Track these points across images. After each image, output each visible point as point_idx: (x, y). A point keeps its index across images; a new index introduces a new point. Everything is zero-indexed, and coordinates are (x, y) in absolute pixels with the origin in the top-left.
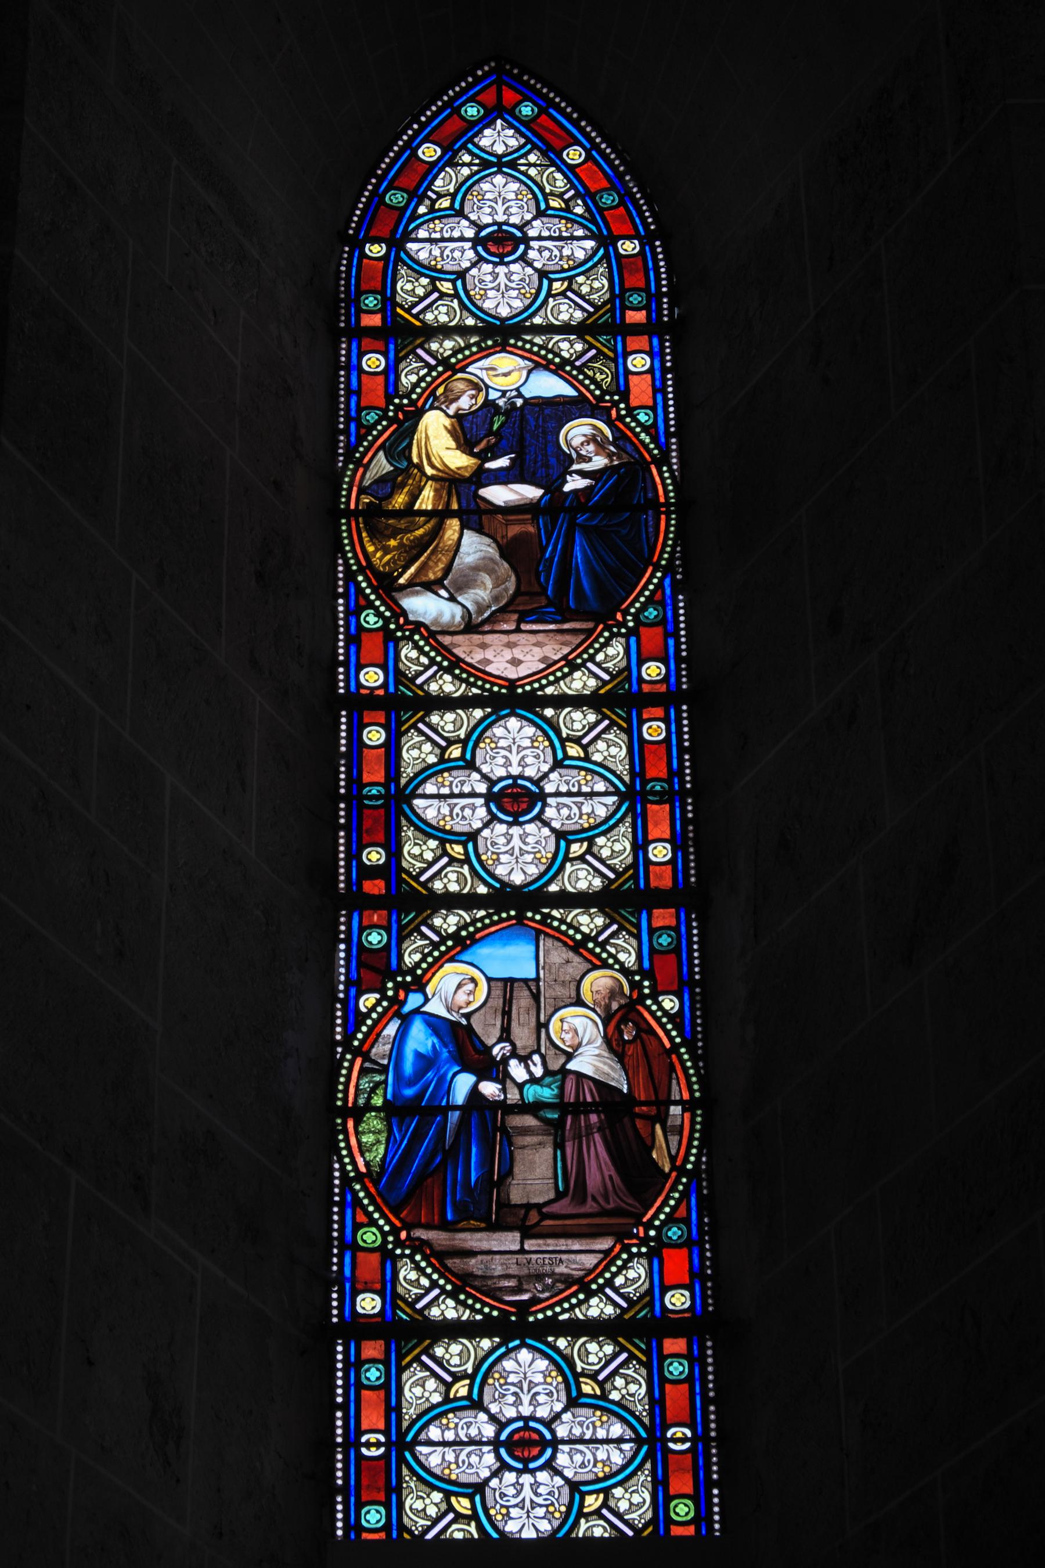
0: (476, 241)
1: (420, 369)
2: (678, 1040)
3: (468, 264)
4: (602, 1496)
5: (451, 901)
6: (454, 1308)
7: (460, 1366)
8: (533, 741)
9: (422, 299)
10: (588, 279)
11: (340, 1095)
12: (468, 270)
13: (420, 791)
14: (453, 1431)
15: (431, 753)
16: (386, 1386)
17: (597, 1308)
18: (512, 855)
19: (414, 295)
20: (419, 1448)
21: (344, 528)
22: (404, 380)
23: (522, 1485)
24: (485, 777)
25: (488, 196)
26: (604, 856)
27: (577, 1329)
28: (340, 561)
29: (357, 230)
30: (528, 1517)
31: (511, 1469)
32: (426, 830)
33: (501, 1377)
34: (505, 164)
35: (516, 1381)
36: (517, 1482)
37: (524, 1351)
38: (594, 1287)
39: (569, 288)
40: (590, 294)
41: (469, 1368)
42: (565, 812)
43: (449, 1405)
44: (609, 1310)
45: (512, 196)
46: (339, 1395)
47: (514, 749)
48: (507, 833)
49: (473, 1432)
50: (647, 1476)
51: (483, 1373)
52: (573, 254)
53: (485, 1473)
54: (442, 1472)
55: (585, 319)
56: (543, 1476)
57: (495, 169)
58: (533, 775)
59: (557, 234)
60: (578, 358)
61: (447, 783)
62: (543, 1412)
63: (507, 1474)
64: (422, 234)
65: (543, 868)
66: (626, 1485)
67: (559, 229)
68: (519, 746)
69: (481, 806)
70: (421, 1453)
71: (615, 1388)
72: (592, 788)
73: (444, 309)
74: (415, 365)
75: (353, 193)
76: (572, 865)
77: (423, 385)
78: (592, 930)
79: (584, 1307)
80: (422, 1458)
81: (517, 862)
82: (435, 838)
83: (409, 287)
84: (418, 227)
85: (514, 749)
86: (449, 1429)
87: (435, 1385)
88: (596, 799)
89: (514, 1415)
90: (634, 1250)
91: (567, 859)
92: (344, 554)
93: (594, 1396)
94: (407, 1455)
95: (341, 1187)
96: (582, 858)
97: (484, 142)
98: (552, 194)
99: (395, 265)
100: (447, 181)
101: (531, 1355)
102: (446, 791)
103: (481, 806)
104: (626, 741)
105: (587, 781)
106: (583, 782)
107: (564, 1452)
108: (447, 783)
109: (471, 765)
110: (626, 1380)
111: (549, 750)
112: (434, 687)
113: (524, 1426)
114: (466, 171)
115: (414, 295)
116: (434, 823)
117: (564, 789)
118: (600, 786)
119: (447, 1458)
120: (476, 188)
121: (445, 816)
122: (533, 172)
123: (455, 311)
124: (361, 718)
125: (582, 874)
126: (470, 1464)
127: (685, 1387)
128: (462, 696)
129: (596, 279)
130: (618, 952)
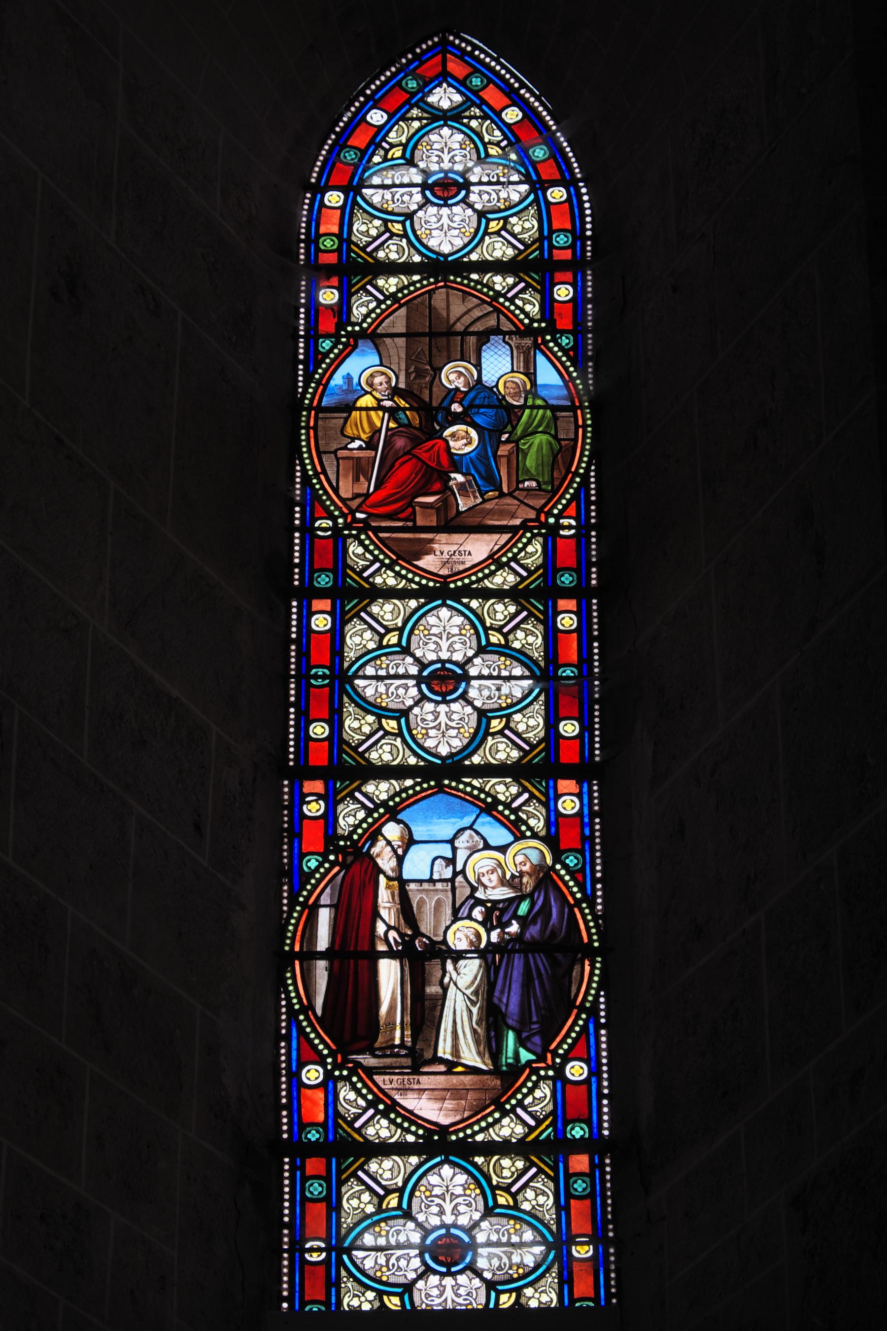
0: (424, 186)
1: (532, 1104)
2: (315, 481)
3: (415, 207)
4: (514, 1295)
5: (386, 772)
6: (387, 1128)
7: (391, 1179)
8: (427, 734)
9: (375, 239)
10: (520, 219)
11: (288, 941)
12: (415, 212)
13: (361, 673)
14: (384, 1238)
15: (518, 722)
16: (327, 1199)
17: (391, 284)
18: (449, 633)
19: (369, 236)
20: (354, 1253)
21: (304, 443)
22: (355, 311)
23: (445, 1287)
24: (417, 660)
25: (436, 146)
26: (520, 731)
27: (407, 268)
28: (298, 468)
29: (319, 179)
30: (447, 1187)
31: (435, 1272)
32: (366, 706)
33: (427, 1190)
34: (452, 117)
35: (439, 1193)
36: (441, 1284)
37: (446, 1167)
38: (508, 1107)
39: (504, 228)
40: (361, 1192)
41: (400, 1181)
42: (486, 693)
43: (381, 1215)
44: (381, 282)
45: (457, 146)
46: (287, 1193)
47: (446, 151)
48: (452, 653)
49: (402, 1238)
50: (554, 1278)
51: (479, 236)
52: (509, 196)
53: (412, 1275)
54: (375, 1274)
55: (516, 256)
56: (434, 167)
57: (442, 122)
58: (427, 704)
59: (495, 180)
60: (509, 290)
61: (384, 666)
62: (463, 1220)
63: (431, 1277)
64: (376, 180)
65: (423, 621)
66: (536, 1286)
67: (497, 174)
68: (439, 730)
69: (413, 686)
70: (356, 1256)
71: (527, 1200)
72: (510, 672)
73: (394, 248)
74: (537, 1108)
75: (314, 137)
76: (396, 624)
77: (373, 315)
78: (385, 572)
79: (400, 285)
80: (358, 1262)
81: (444, 627)
82: (373, 714)
83: (364, 228)
84: (371, 175)
85: (446, 151)
86: (381, 1236)
87: (514, 228)
88: (513, 682)
89: (439, 1223)
90: (542, 1073)
91: (401, 630)
92: (302, 460)
93: (508, 1207)
94: (345, 1257)
95: (288, 1020)
96: (388, 630)
97: (431, 99)
98: (490, 143)
99: (352, 209)
100: (400, 133)
101: (452, 1170)
102: (382, 673)
103: (413, 686)
104: (344, 733)
105: (380, 697)
106: (503, 667)
107: (482, 1256)
108: (384, 666)
109: (406, 651)
110: (535, 1192)
111: (412, 726)
112: (378, 580)
113: (448, 1228)
114: (416, 124)
115: (369, 236)
116: (372, 700)
117: (486, 672)
118: (518, 671)
119: (379, 1261)
120: (426, 138)
121: (382, 694)
122: (474, 124)
123: (404, 250)
124: (310, 606)
125: (501, 747)
126: (399, 1267)
127: (588, 1202)
128: (402, 589)
129: (528, 220)
130: (364, 554)
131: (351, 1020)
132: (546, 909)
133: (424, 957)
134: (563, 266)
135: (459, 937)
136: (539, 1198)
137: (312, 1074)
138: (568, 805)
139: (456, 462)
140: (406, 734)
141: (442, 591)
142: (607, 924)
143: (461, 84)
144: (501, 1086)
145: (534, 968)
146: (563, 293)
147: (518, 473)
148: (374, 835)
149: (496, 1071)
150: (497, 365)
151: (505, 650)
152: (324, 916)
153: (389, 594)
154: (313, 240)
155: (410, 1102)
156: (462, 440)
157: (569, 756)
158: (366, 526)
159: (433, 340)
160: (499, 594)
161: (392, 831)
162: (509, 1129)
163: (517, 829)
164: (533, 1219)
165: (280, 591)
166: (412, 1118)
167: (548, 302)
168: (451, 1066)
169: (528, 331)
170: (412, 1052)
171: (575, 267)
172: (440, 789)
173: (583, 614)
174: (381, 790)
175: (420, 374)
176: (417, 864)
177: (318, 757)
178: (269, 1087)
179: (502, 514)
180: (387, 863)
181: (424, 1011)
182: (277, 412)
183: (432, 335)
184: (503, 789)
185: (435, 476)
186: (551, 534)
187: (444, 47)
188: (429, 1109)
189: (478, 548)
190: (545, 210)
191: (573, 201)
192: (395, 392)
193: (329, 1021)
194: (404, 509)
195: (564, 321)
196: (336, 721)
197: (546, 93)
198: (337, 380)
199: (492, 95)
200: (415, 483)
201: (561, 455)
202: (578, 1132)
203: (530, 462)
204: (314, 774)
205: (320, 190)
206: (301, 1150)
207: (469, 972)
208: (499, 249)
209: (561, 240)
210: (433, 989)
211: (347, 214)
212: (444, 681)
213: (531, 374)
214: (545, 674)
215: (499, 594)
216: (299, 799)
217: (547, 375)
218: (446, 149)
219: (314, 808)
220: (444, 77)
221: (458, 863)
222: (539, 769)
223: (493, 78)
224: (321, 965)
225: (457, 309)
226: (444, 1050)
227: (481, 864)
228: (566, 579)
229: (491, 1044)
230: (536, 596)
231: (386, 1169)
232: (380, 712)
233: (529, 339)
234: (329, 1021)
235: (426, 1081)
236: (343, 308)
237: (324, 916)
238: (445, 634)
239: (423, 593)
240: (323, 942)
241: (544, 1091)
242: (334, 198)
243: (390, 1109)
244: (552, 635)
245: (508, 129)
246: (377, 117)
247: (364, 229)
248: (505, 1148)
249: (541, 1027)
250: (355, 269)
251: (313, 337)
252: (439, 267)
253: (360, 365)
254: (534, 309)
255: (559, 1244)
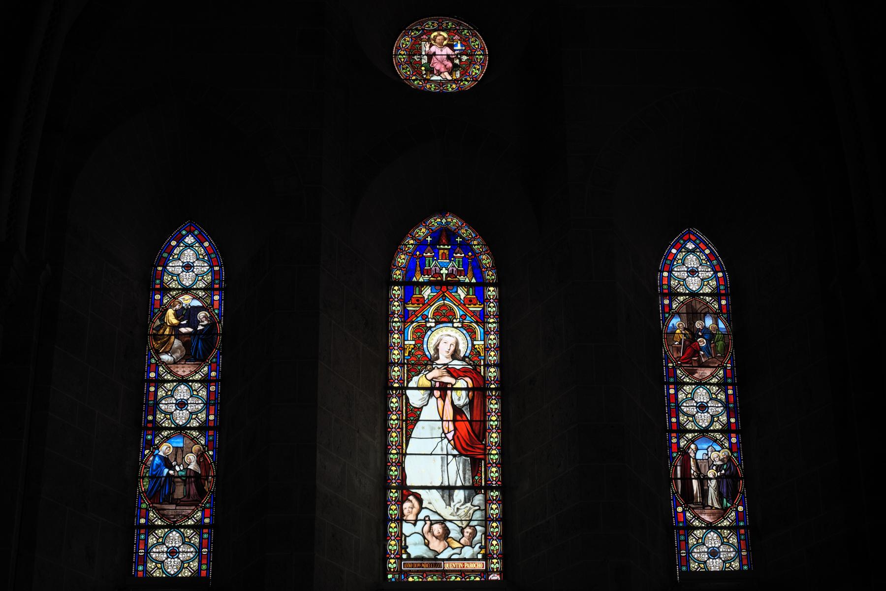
5: (691, 431)
27: (685, 294)
34: (692, 251)
131: (687, 495)
132: (730, 467)
133: (703, 480)
134: (723, 295)
135: (710, 474)
136: (733, 540)
137: (680, 509)
138: (734, 440)
139: (701, 349)
140: (694, 421)
141: (700, 383)
142: (745, 471)
143: (694, 242)
144: (723, 513)
145: (729, 483)
146: (724, 302)
147: (716, 352)
148: (689, 448)
149: (722, 509)
150: (709, 322)
151: (716, 399)
152: (679, 468)
153: (688, 384)
154: (661, 286)
155: (703, 516)
156: (702, 342)
157: (733, 428)
158: (681, 366)
159: (692, 314)
160: (714, 384)
161: (693, 446)
162: (726, 523)
163: (722, 446)
164: (732, 545)
165: (662, 383)
166: (703, 520)
167: (720, 305)
168: (712, 507)
169: (715, 313)
170: (703, 504)
171: (726, 296)
172: (704, 436)
173: (734, 390)
174: (690, 436)
175: (691, 324)
176: (699, 455)
177: (675, 427)
178: (668, 515)
179: (713, 363)
180: (692, 455)
181: (704, 493)
182: (656, 335)
183: (693, 313)
184: (718, 436)
185: (696, 352)
186: (725, 369)
187: (689, 232)
188: (706, 518)
189: (708, 372)
190: (718, 279)
191: (724, 276)
192: (685, 329)
193: (682, 495)
194: (690, 361)
195: (724, 311)
196: (678, 418)
197: (716, 246)
198: (671, 325)
199: (702, 245)
200: (692, 357)
201: (726, 347)
202: (742, 524)
203: (719, 349)
204: (674, 431)
205: (662, 272)
206: (679, 528)
207: (714, 482)
208: (707, 290)
209: (722, 287)
210: (706, 488)
211: (669, 278)
212: (702, 407)
213: (717, 325)
214: (726, 406)
215: (714, 384)
216: (671, 439)
217: (721, 325)
218: (692, 261)
219: (674, 441)
220: (689, 240)
221: (710, 454)
222: (726, 431)
223: (702, 241)
224: (679, 481)
225: (698, 306)
226: (710, 503)
227: (714, 455)
228: (729, 381)
229: (720, 502)
230: (722, 385)
231: (698, 533)
232: (688, 415)
233: (716, 316)
234: (682, 495)
235: (706, 511)
236: (670, 305)
237: (679, 468)
238: (702, 395)
239: (695, 384)
240: (679, 476)
241: (733, 514)
242: (665, 274)
243: (699, 518)
244: (727, 395)
245: (706, 255)
246: (674, 251)
247: (674, 283)
248: (725, 528)
249: (732, 498)
250: (673, 294)
251: (664, 313)
252: (693, 294)
253: (675, 321)
254: (717, 307)
255: (738, 551)
